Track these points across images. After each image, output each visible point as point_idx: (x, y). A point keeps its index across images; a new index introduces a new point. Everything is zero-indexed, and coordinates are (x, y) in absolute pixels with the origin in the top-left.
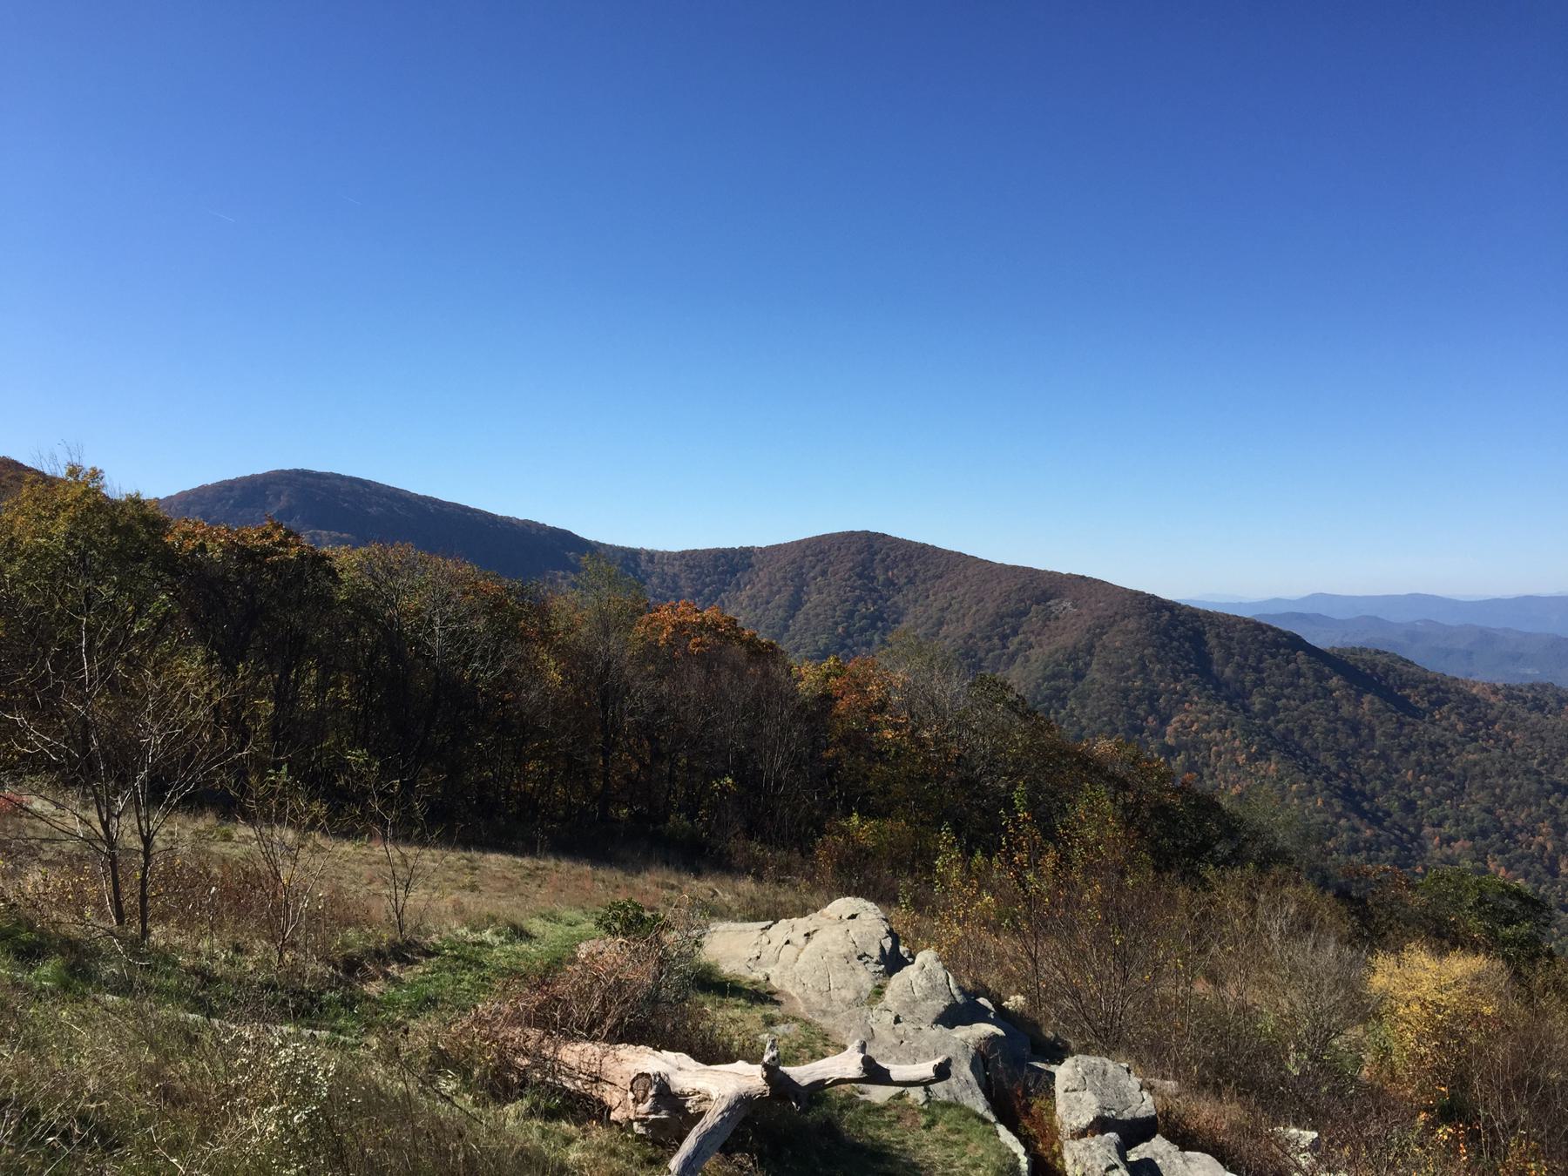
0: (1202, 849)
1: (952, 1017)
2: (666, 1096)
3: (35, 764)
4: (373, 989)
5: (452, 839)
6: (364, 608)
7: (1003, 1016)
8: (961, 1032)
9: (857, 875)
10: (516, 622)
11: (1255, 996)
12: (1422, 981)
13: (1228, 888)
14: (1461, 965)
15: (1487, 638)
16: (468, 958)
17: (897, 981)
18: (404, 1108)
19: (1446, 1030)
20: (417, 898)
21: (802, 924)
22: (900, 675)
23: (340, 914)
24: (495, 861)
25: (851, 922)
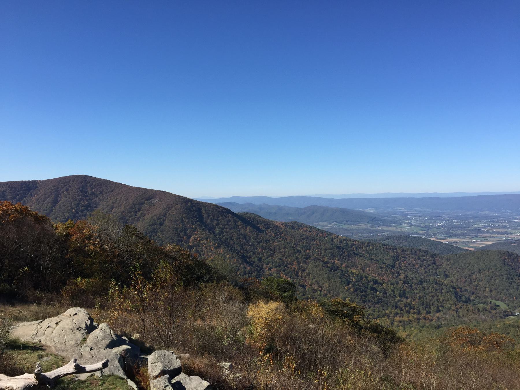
0: (200, 278)
1: (111, 345)
7: (131, 342)
9: (79, 299)
11: (215, 323)
12: (262, 311)
13: (207, 290)
14: (273, 305)
15: (280, 208)
17: (92, 335)
19: (268, 326)
21: (55, 319)
25: (75, 316)
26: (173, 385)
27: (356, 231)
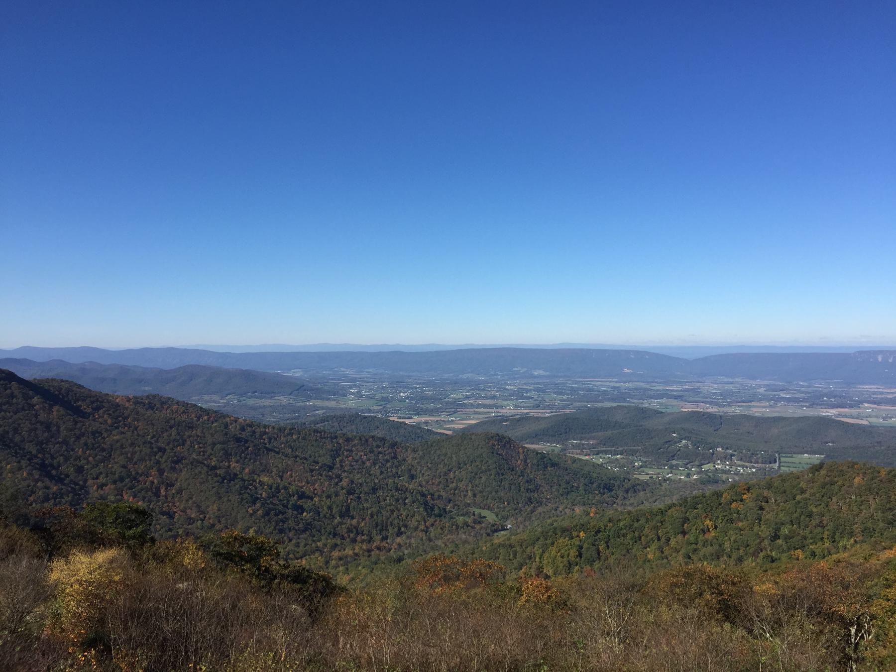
14: (102, 556)
15: (124, 371)
19: (93, 595)
27: (270, 410)
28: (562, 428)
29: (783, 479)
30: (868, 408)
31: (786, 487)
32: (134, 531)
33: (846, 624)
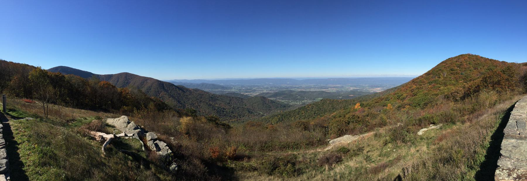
0: (163, 108)
1: (135, 129)
2: (102, 137)
3: (35, 98)
4: (70, 124)
5: (78, 108)
6: (68, 82)
7: (141, 128)
8: (136, 130)
9: (125, 113)
10: (85, 83)
11: (169, 124)
12: (185, 120)
13: (166, 112)
14: (189, 118)
15: (191, 84)
16: (80, 121)
17: (129, 125)
18: (74, 137)
19: (187, 125)
20: (75, 114)
21: (118, 119)
22: (130, 90)
23: (66, 115)
24: (83, 110)
25: (124, 119)
26: (155, 144)
27: (217, 92)
28: (276, 95)
29: (316, 103)
30: (330, 89)
31: (316, 104)
32: (193, 114)
33: (325, 128)
